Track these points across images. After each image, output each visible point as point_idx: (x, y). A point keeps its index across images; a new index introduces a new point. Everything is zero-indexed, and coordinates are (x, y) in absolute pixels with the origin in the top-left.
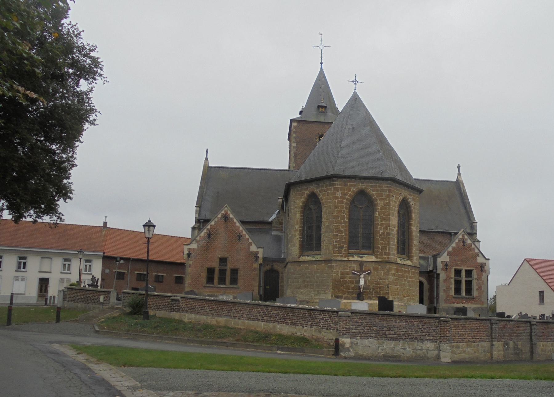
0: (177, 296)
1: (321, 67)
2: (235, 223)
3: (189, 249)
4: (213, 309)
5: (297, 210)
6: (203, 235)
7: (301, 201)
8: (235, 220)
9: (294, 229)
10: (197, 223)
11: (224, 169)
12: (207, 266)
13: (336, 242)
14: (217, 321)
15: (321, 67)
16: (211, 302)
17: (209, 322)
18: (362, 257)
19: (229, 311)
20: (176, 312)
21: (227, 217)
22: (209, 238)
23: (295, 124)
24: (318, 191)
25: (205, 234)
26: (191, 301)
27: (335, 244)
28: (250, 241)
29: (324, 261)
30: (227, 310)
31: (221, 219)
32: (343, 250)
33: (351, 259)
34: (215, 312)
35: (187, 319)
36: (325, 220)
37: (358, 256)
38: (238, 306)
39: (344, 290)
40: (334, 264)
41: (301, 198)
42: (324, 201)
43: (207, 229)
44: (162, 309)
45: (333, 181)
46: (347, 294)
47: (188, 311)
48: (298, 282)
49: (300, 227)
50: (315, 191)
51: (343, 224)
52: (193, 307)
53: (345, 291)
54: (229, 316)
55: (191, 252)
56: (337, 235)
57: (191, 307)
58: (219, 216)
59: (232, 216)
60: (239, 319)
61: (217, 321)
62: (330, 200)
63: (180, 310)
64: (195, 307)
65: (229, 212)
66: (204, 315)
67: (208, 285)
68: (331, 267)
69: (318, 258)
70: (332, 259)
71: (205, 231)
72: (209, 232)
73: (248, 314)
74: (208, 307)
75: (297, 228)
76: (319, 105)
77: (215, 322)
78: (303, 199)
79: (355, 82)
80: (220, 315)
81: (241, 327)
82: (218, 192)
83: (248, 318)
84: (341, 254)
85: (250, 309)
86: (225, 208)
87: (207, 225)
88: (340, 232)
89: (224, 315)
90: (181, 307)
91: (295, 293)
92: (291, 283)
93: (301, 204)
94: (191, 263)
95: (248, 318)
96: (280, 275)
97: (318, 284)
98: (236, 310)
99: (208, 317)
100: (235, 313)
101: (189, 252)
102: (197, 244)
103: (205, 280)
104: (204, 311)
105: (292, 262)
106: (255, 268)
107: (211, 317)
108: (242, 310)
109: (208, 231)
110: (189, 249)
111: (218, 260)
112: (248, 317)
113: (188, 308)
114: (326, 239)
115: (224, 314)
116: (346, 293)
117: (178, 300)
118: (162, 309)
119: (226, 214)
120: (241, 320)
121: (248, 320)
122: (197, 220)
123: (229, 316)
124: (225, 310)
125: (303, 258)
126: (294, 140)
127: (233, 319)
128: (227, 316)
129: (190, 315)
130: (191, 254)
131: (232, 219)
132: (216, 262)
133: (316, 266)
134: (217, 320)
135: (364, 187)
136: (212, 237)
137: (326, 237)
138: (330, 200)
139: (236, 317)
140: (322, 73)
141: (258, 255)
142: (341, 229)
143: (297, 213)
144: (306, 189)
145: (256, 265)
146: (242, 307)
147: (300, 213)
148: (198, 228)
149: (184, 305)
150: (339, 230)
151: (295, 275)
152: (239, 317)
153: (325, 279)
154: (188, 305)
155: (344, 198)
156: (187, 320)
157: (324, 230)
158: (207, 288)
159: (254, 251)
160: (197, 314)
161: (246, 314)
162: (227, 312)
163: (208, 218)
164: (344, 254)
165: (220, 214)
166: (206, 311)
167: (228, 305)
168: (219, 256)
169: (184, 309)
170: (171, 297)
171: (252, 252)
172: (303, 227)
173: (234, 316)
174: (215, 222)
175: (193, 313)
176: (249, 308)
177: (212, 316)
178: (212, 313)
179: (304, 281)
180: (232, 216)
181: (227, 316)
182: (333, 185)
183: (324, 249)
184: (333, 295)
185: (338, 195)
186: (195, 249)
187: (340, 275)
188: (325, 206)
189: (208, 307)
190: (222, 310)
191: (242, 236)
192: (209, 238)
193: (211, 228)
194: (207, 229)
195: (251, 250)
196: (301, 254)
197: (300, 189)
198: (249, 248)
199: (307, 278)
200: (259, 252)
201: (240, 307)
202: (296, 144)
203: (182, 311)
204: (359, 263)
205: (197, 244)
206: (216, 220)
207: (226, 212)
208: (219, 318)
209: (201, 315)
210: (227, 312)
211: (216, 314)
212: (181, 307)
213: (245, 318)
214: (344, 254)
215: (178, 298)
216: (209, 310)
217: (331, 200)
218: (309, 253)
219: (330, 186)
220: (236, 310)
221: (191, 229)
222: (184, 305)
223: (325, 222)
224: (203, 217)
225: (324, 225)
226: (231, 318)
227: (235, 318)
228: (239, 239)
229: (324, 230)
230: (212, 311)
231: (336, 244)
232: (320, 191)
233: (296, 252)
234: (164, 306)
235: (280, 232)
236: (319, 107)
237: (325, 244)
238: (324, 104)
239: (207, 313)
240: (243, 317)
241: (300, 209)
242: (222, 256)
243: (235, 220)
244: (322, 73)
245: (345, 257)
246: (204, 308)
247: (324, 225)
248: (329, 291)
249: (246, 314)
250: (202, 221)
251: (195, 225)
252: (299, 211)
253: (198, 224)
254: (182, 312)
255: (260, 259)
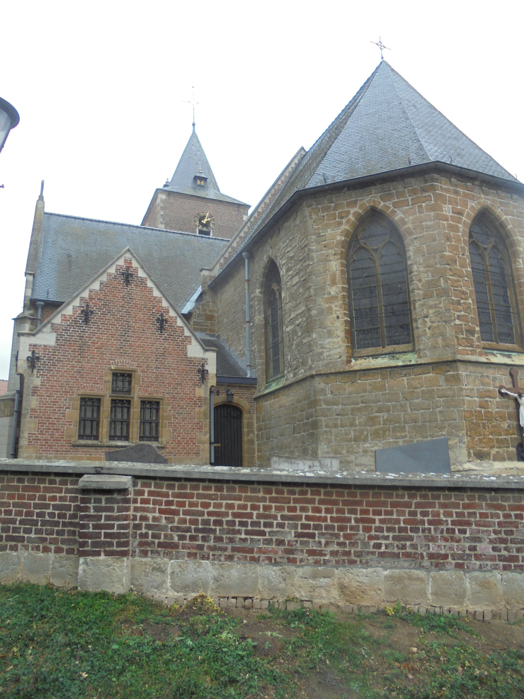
0: (111, 473)
1: (194, 130)
2: (151, 290)
3: (33, 347)
4: (316, 527)
5: (331, 251)
6: (71, 314)
7: (339, 231)
8: (150, 284)
9: (326, 296)
10: (29, 309)
11: (77, 220)
12: (81, 392)
13: (459, 317)
14: (342, 588)
15: (194, 130)
16: (302, 493)
17: (302, 594)
18: (509, 357)
19: (401, 530)
20: (108, 554)
21: (132, 275)
22: (86, 321)
23: (162, 197)
24: (388, 204)
25: (75, 311)
26: (192, 496)
27: (457, 322)
28: (187, 333)
29: (430, 367)
30: (389, 530)
31: (115, 278)
32: (475, 339)
33: (494, 360)
34: (327, 544)
35: (174, 587)
36: (422, 269)
37: (504, 355)
38: (443, 506)
39: (491, 436)
40: (463, 371)
41: (340, 224)
42: (410, 225)
43: (82, 299)
44: (22, 539)
45: (432, 180)
46: (498, 448)
47: (176, 546)
48: (352, 425)
49: (343, 291)
50: (381, 205)
51: (466, 279)
52: (206, 522)
53: (492, 439)
54: (408, 555)
55: (40, 353)
56: (459, 303)
57: (194, 522)
58: (112, 270)
59: (141, 274)
60: (459, 566)
61: (342, 588)
62: (429, 223)
63: (134, 543)
64: (218, 523)
65: (135, 264)
66: (272, 562)
67: (83, 442)
68: (457, 379)
69: (412, 359)
70: (459, 357)
71: (77, 303)
72: (87, 306)
73: (503, 541)
74: (362, 520)
75: (333, 293)
76: (197, 175)
77: (335, 593)
78: (345, 227)
79: (381, 46)
80: (359, 554)
81: (479, 609)
82: (69, 256)
83: (502, 558)
84: (471, 346)
85: (506, 516)
86: (125, 253)
87: (55, 313)
88: (463, 296)
89: (382, 555)
90: (137, 527)
91: (344, 452)
92: (327, 426)
93: (340, 238)
94: (37, 382)
95: (502, 558)
96: (245, 415)
97: (420, 424)
98: (436, 522)
99: (291, 568)
100: (433, 539)
101: (33, 352)
102: (55, 335)
103: (74, 429)
104: (269, 542)
105: (327, 375)
106: (200, 399)
107: (307, 570)
108: (469, 524)
109: (84, 305)
110: (33, 347)
111: (110, 378)
112: (504, 553)
113: (178, 529)
114: (431, 311)
115: (378, 546)
116: (496, 445)
117: (123, 491)
118: (22, 539)
119: (128, 268)
120: (469, 570)
121: (505, 568)
122: (28, 302)
123: (408, 555)
124: (379, 529)
125: (357, 364)
126: (161, 220)
127: (428, 570)
128: (397, 556)
129: (191, 564)
130: (38, 358)
131: (143, 281)
132: (106, 382)
133: (405, 378)
134: (346, 581)
135: (489, 202)
136: (93, 319)
137: (431, 307)
138: (429, 223)
139: (446, 556)
140: (194, 135)
141: (206, 367)
142: (464, 289)
143: (332, 258)
144: (354, 204)
145: (202, 392)
146: (466, 506)
147: (341, 258)
148: (30, 319)
149: (150, 515)
150: (460, 291)
151: (340, 407)
152: (461, 557)
153: (440, 412)
154: (176, 513)
155: (459, 221)
156: (172, 594)
157: (421, 292)
158: (80, 449)
159: (195, 358)
160: (230, 558)
161: (491, 541)
162: (394, 538)
163: (53, 298)
164: (477, 347)
165: (114, 267)
166: (280, 543)
167: (394, 505)
168: (113, 367)
169: (154, 536)
170: (80, 475)
171: (191, 361)
172: (349, 291)
173: (431, 556)
174: (101, 284)
175: (205, 557)
176: (501, 507)
177: (317, 563)
178: (313, 546)
179: (372, 420)
180: (141, 274)
181: (397, 556)
182: (433, 188)
183: (429, 335)
184: (471, 451)
185: (446, 212)
186: (51, 347)
187: (476, 399)
188: (414, 236)
189: (362, 520)
190: (367, 529)
191: (166, 321)
192: (86, 321)
193: (91, 298)
194: (82, 299)
195: (189, 355)
196: (352, 356)
197: (333, 205)
198: (184, 351)
199: (380, 411)
200: (209, 362)
201: (457, 506)
202: (164, 225)
203: (141, 544)
204: (509, 369)
205: (55, 335)
206: (104, 278)
207: (128, 262)
208: (355, 570)
209: (254, 560)
210: (394, 538)
211: (334, 553)
212: (137, 527)
213: (492, 559)
214: (477, 347)
215: (126, 481)
216: (298, 535)
217: (432, 223)
218: (371, 350)
219: (424, 190)
220: (440, 522)
221: (13, 321)
222: (150, 515)
223: (423, 272)
224: (41, 295)
225: (420, 281)
226: (421, 567)
227: (438, 566)
228: (161, 328)
229: (421, 292)
230: (312, 536)
231: (459, 323)
232: (395, 205)
233: (338, 350)
234: (35, 523)
235: (207, 334)
236: (196, 178)
237: (429, 324)
238: (202, 175)
239: (287, 551)
240: (478, 557)
241: (339, 250)
242: (120, 366)
243: (150, 284)
244: (194, 135)
245: (481, 355)
246: (270, 525)
247: (420, 281)
248: (460, 441)
249: (491, 541)
250: (42, 303)
251: (23, 313)
252: (335, 254)
253: (31, 312)
254: (145, 554)
255: (210, 376)
